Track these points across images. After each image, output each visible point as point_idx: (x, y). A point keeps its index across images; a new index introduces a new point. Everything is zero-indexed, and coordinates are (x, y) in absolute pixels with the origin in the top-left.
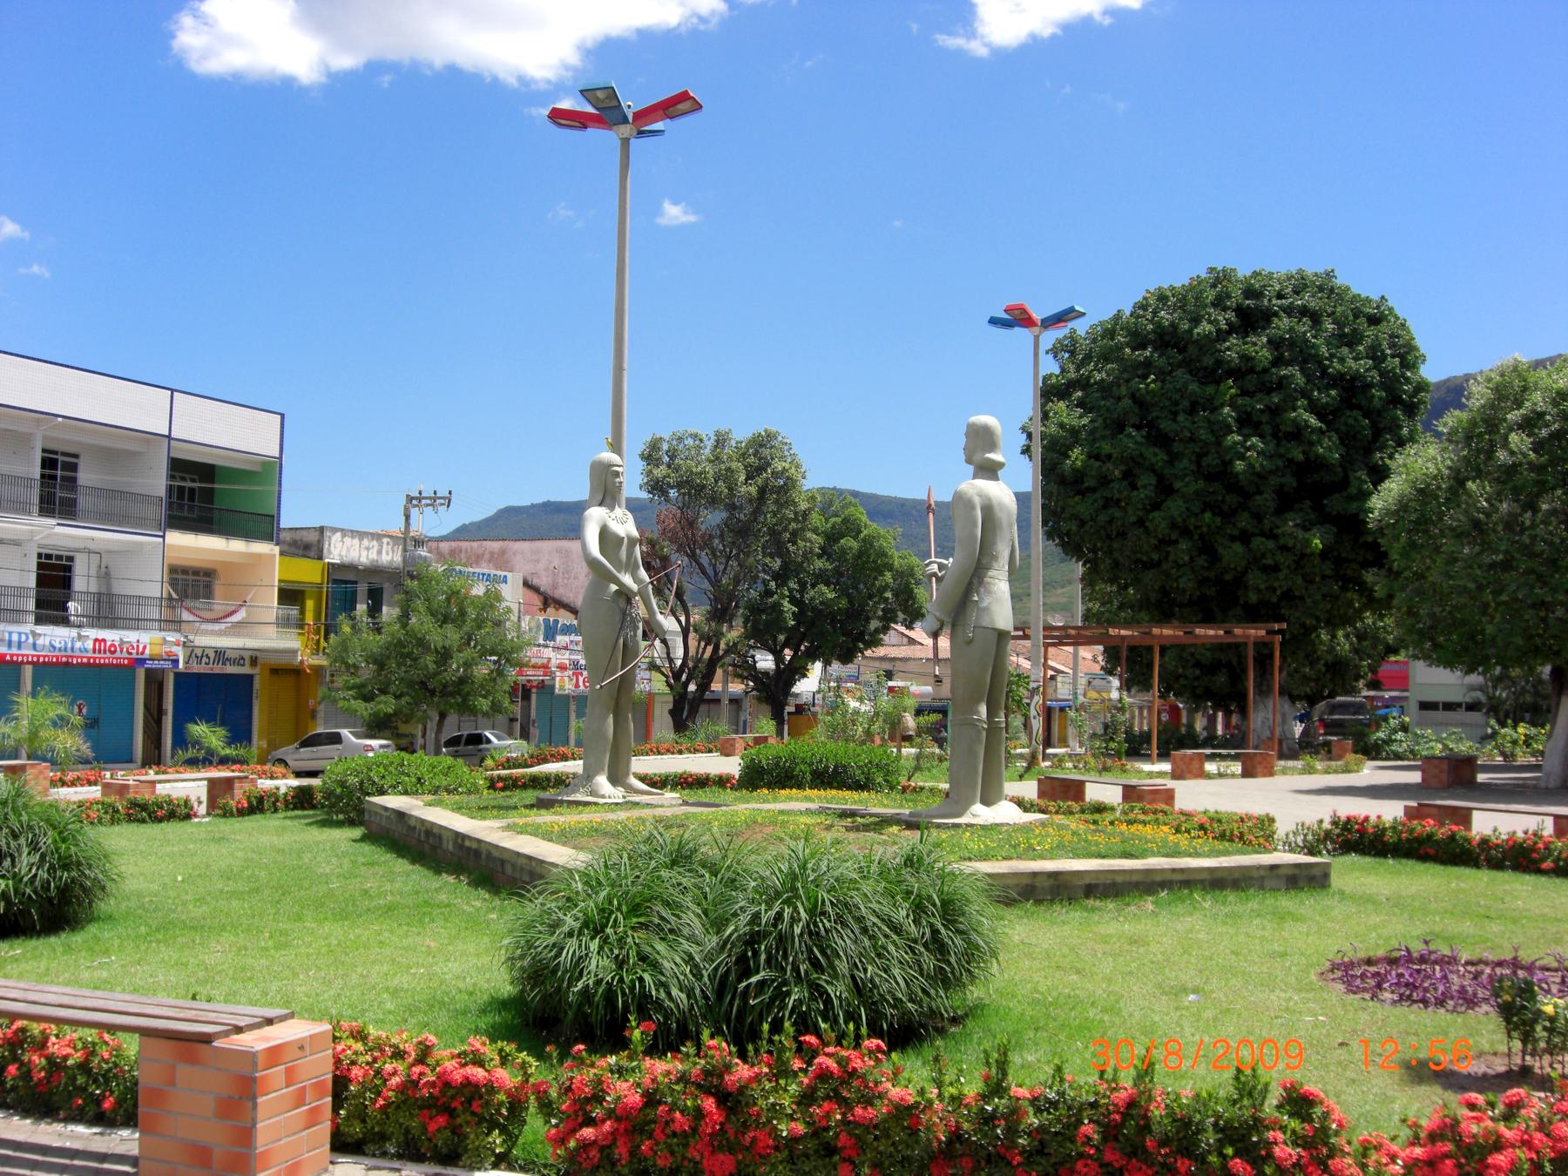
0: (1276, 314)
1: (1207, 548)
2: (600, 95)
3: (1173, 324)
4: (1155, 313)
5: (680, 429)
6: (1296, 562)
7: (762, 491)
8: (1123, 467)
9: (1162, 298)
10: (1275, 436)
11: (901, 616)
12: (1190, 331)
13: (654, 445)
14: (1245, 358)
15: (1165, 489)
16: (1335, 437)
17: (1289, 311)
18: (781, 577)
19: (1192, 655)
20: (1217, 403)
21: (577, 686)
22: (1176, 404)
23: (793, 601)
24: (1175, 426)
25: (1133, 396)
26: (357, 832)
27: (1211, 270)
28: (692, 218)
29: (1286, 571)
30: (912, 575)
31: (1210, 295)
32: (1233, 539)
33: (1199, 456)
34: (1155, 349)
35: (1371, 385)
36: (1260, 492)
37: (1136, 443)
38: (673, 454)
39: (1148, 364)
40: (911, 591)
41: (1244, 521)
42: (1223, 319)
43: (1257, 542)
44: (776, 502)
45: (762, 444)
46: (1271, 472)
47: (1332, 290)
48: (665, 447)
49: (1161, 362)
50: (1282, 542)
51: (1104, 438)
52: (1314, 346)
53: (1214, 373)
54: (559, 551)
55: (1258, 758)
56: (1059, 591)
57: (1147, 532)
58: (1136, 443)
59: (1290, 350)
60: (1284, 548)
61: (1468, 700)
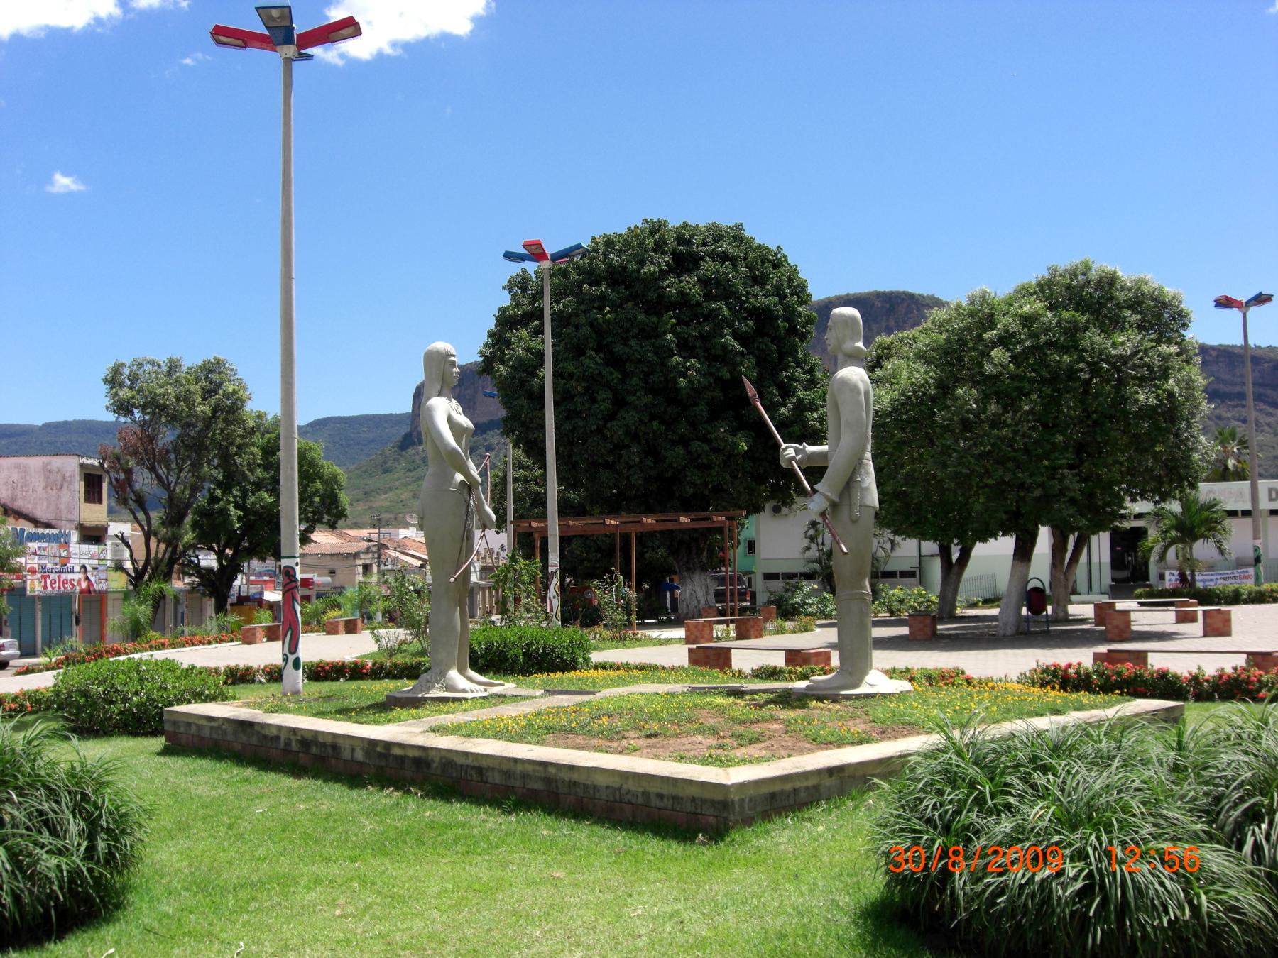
0: (702, 258)
1: (652, 451)
2: (275, 13)
3: (621, 265)
4: (605, 256)
5: (140, 355)
6: (724, 461)
7: (215, 410)
8: (584, 384)
9: (609, 243)
10: (707, 358)
11: (326, 518)
12: (638, 271)
13: (116, 371)
14: (682, 293)
15: (620, 402)
16: (753, 359)
17: (713, 256)
18: (226, 486)
19: (595, 542)
20: (661, 330)
21: (45, 587)
22: (627, 331)
23: (237, 506)
24: (627, 350)
25: (591, 325)
26: (158, 743)
27: (645, 221)
28: (82, 188)
29: (717, 469)
30: (336, 482)
31: (650, 242)
32: (673, 443)
33: (647, 375)
34: (608, 285)
35: (777, 318)
36: (696, 405)
37: (596, 363)
38: (134, 378)
39: (603, 297)
40: (336, 496)
41: (683, 428)
42: (664, 261)
43: (696, 445)
44: (225, 421)
45: (212, 373)
46: (704, 388)
47: (742, 239)
48: (127, 372)
49: (613, 296)
50: (714, 444)
51: (566, 359)
52: (733, 285)
53: (660, 305)
54: (17, 467)
55: (752, 623)
56: (383, 497)
57: (605, 438)
58: (596, 363)
59: (717, 288)
60: (716, 450)
61: (807, 570)
